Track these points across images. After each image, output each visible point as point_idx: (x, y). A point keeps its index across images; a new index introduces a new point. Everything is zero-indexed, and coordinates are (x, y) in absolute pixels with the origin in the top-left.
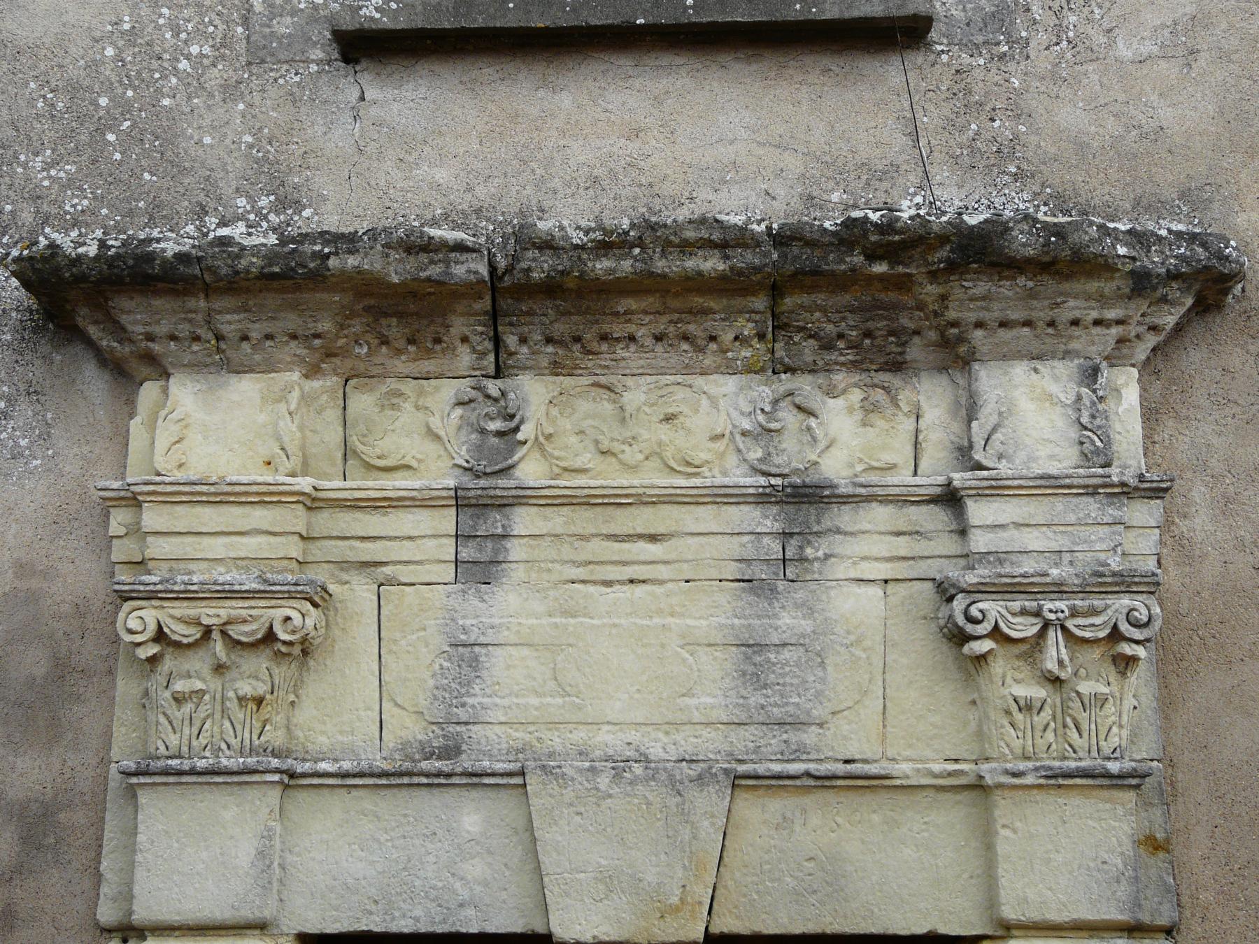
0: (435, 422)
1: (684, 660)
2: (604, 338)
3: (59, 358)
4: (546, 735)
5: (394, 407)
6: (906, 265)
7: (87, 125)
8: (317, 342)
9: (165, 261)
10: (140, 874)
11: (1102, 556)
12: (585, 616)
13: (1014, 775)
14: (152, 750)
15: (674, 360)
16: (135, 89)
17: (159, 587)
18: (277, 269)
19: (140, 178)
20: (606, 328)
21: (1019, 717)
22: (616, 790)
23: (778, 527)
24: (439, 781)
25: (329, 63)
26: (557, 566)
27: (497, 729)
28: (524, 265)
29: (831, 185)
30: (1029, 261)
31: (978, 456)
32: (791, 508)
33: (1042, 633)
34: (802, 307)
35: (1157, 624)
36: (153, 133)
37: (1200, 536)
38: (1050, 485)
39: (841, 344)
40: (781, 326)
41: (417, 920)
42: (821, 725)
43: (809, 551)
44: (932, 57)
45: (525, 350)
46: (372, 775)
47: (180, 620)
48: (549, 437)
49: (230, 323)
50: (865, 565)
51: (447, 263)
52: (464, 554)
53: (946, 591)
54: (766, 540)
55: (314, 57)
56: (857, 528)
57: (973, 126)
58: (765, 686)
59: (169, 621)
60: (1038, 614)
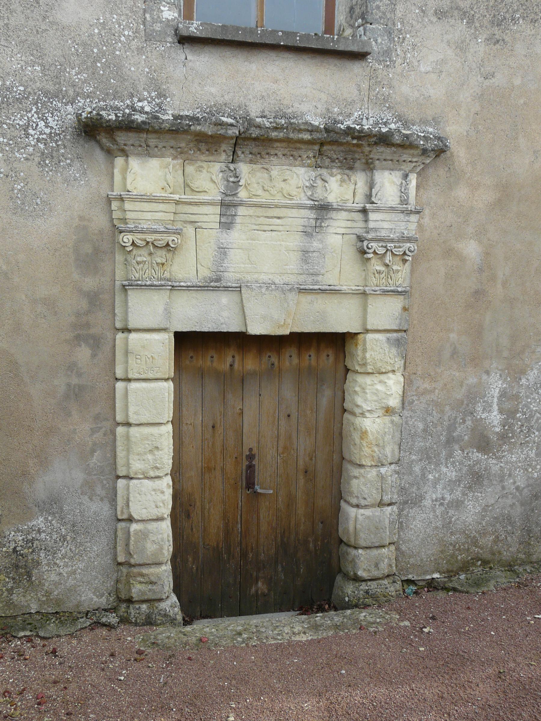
0: (214, 178)
1: (286, 255)
2: (268, 154)
3: (87, 146)
4: (246, 276)
5: (200, 171)
6: (362, 141)
7: (90, 59)
8: (179, 149)
9: (138, 123)
10: (130, 315)
11: (403, 231)
12: (258, 240)
13: (375, 291)
14: (130, 278)
15: (287, 162)
16: (106, 46)
17: (134, 229)
18: (174, 128)
19: (110, 81)
20: (269, 151)
21: (377, 275)
22: (267, 293)
23: (315, 216)
24: (216, 289)
25: (174, 43)
26: (250, 225)
27: (232, 273)
28: (250, 132)
29: (335, 105)
30: (397, 144)
31: (373, 199)
32: (319, 211)
33: (386, 253)
34: (329, 150)
35: (416, 252)
36: (114, 64)
37: (426, 224)
38: (392, 209)
39: (337, 161)
40: (321, 153)
41: (209, 328)
42: (323, 275)
43: (323, 224)
44: (367, 64)
45: (243, 156)
46: (196, 287)
47: (139, 239)
48: (249, 184)
49: (152, 142)
50: (338, 229)
51: (226, 129)
52: (222, 220)
53: (360, 239)
54: (311, 220)
55: (168, 40)
56: (337, 218)
57: (377, 90)
58: (308, 263)
59: (136, 239)
60: (386, 247)
